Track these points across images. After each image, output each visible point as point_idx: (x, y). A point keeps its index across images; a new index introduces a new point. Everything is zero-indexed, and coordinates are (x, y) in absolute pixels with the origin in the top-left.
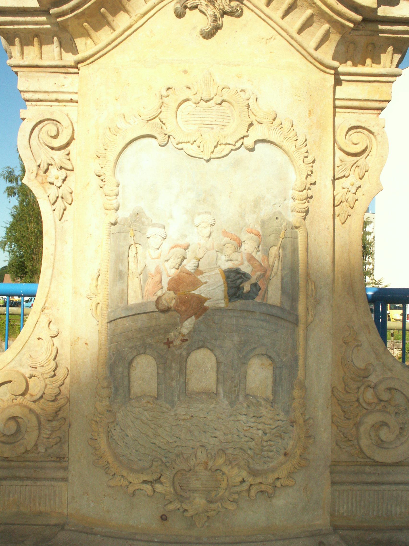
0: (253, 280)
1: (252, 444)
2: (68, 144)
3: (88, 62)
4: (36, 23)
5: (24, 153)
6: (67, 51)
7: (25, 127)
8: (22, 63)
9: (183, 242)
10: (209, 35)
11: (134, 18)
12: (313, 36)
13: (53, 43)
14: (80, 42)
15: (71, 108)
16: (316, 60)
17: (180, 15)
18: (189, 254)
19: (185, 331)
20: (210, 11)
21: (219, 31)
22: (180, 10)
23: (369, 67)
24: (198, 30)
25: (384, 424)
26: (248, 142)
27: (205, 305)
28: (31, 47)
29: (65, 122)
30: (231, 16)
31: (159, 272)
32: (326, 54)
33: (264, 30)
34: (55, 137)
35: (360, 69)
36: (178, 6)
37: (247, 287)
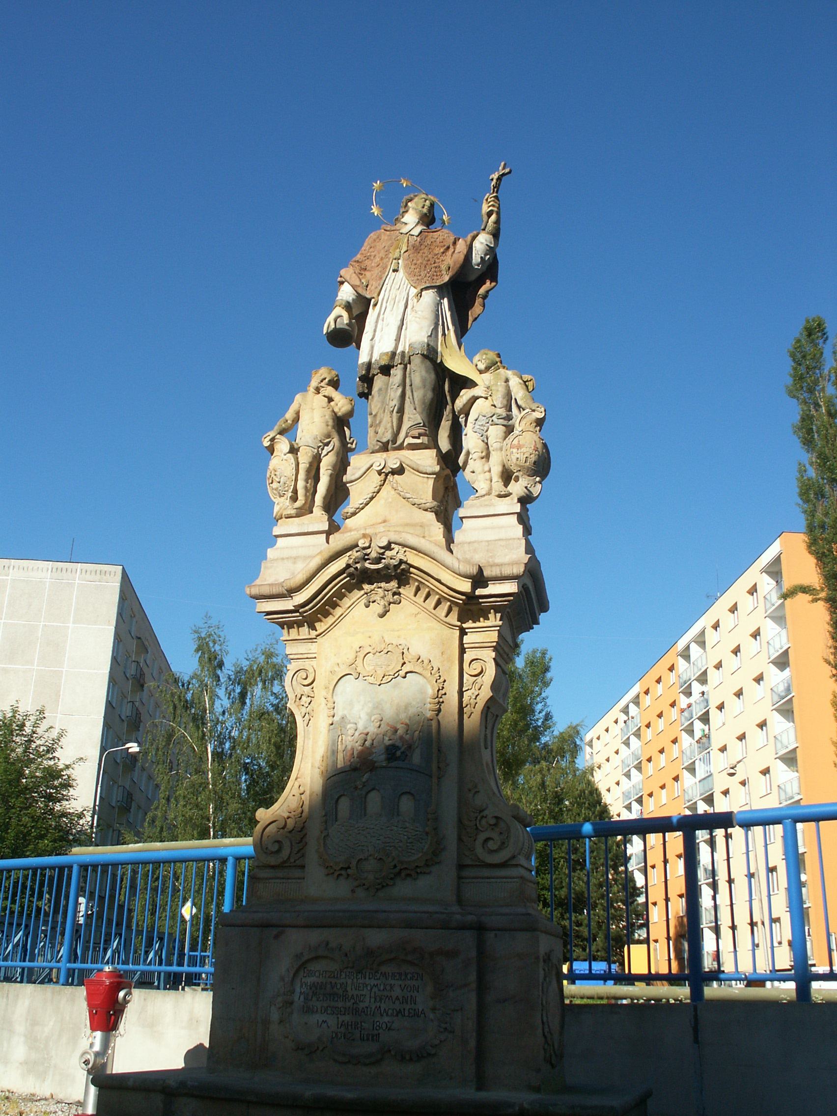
0: (402, 749)
1: (401, 844)
2: (312, 683)
4: (310, 609)
5: (288, 689)
7: (289, 674)
9: (365, 731)
10: (382, 616)
14: (317, 625)
15: (314, 663)
17: (367, 606)
18: (369, 738)
19: (364, 780)
20: (382, 602)
23: (482, 623)
25: (487, 840)
26: (402, 673)
29: (311, 670)
31: (353, 749)
32: (453, 618)
33: (413, 609)
34: (306, 679)
37: (398, 753)
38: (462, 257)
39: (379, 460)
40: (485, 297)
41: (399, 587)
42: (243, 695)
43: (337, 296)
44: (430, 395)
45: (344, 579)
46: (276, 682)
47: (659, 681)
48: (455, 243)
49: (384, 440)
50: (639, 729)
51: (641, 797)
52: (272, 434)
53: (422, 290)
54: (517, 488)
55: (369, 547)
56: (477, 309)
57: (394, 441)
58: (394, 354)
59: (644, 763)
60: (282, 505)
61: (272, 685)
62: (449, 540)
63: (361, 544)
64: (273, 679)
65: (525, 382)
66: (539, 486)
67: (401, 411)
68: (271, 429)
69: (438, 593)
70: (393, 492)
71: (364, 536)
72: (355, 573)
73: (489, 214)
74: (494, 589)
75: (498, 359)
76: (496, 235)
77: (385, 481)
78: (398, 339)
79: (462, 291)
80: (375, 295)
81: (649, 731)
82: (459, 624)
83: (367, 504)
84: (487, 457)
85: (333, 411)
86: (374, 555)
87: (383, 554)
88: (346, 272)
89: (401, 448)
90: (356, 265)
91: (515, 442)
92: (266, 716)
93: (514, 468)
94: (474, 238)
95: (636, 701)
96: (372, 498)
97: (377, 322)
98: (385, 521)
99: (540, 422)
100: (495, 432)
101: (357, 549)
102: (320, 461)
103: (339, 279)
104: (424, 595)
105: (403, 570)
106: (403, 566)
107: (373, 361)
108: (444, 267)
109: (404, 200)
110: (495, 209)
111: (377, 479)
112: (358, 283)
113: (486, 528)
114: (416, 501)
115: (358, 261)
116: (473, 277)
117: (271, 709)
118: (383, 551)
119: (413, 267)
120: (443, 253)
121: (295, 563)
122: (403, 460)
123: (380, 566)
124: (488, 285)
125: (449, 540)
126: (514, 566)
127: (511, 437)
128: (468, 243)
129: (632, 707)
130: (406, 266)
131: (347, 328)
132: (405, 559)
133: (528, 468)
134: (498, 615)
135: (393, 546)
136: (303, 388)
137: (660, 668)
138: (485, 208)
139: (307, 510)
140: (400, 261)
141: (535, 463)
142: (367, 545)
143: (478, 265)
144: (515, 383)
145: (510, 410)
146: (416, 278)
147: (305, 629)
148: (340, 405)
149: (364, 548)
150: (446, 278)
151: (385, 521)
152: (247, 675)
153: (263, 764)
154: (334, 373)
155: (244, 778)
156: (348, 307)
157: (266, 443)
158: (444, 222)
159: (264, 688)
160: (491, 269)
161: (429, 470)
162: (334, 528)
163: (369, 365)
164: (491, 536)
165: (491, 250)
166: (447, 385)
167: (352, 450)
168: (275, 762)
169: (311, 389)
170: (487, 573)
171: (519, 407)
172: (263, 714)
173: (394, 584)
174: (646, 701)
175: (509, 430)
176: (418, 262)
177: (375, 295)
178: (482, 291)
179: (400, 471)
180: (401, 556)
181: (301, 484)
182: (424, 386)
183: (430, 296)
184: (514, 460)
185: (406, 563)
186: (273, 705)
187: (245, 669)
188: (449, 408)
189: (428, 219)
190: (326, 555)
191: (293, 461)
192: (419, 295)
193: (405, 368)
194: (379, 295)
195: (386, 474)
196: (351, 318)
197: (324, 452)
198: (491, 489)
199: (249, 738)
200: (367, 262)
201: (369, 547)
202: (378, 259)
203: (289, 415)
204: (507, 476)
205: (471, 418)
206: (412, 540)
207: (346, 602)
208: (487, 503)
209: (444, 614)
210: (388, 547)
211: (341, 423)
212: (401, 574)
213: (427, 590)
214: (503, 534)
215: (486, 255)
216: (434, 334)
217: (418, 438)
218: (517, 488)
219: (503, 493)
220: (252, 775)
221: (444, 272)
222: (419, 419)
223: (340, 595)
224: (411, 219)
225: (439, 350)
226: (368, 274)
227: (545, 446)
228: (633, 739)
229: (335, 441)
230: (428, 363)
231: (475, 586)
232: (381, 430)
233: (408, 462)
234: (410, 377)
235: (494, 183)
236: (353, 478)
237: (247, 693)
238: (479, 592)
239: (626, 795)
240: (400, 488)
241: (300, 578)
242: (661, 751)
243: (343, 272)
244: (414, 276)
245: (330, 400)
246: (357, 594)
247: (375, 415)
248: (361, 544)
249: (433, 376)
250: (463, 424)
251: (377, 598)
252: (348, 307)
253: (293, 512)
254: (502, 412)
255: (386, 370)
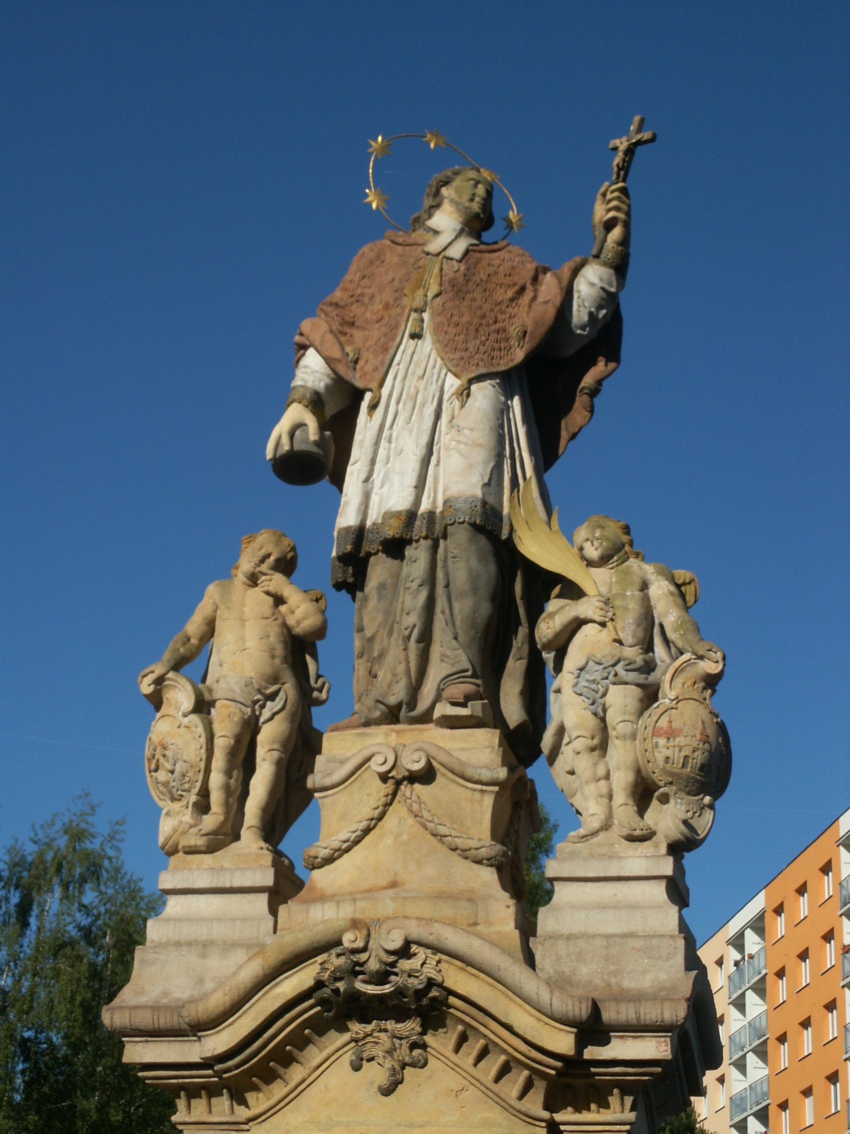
3: (260, 1120)
6: (239, 1104)
8: (187, 1119)
10: (388, 1091)
11: (308, 1071)
12: (515, 1082)
13: (222, 1095)
14: (250, 1097)
16: (519, 1111)
17: (357, 1068)
20: (388, 1063)
21: (400, 1086)
22: (357, 1063)
24: (376, 1086)
27: (692, 1098)
28: (198, 1100)
30: (415, 1067)
32: (534, 1104)
33: (453, 1080)
35: (585, 1116)
36: (354, 1058)
38: (551, 313)
39: (383, 744)
40: (594, 392)
41: (424, 1033)
42: (24, 909)
43: (293, 376)
44: (486, 608)
45: (310, 1010)
46: (88, 886)
47: (801, 890)
48: (535, 280)
49: (393, 700)
50: (763, 979)
51: (766, 1108)
52: (158, 670)
53: (471, 382)
54: (667, 818)
55: (364, 949)
56: (577, 415)
57: (412, 703)
58: (411, 516)
59: (772, 1044)
60: (174, 820)
61: (81, 893)
62: (527, 927)
63: (348, 940)
64: (83, 880)
65: (678, 586)
66: (708, 815)
67: (426, 638)
68: (157, 659)
69: (504, 1051)
70: (411, 821)
71: (355, 924)
72: (334, 998)
73: (609, 225)
74: (622, 1048)
75: (625, 539)
76: (620, 267)
77: (394, 794)
78: (420, 486)
79: (548, 381)
80: (374, 385)
81: (782, 984)
82: (546, 1115)
83: (357, 842)
84: (602, 747)
85: (285, 625)
86: (373, 965)
87: (393, 964)
88: (313, 327)
89: (425, 718)
90: (333, 312)
91: (663, 723)
92: (68, 951)
93: (659, 778)
94: (575, 272)
95: (758, 925)
96: (367, 831)
97: (377, 443)
98: (394, 885)
99: (711, 682)
100: (621, 700)
101: (338, 950)
102: (256, 730)
103: (297, 338)
104: (475, 1053)
105: (434, 999)
106: (434, 993)
107: (369, 523)
108: (514, 331)
109: (433, 182)
110: (621, 216)
111: (378, 791)
112: (336, 353)
113: (602, 907)
114: (459, 842)
115: (337, 305)
116: (570, 350)
117: (74, 933)
118: (392, 959)
119: (452, 330)
120: (512, 300)
121: (203, 956)
122: (433, 752)
123: (387, 989)
124: (600, 368)
125: (527, 927)
126: (667, 1005)
127: (655, 710)
128: (565, 283)
129: (751, 937)
130: (437, 329)
131: (315, 449)
132: (439, 979)
133: (689, 779)
134: (629, 1100)
135: (414, 948)
136: (223, 571)
137: (805, 866)
138: (600, 212)
139: (227, 834)
140: (426, 316)
141: (702, 767)
142: (360, 944)
143: (583, 328)
144: (660, 589)
145: (648, 647)
146: (458, 355)
147: (223, 1103)
148: (299, 613)
149: (354, 951)
150: (519, 355)
151: (394, 885)
152: (34, 872)
153: (56, 1039)
154: (286, 542)
155: (20, 1067)
156: (316, 402)
157: (146, 687)
158: (510, 225)
159: (66, 897)
160: (607, 336)
161: (486, 775)
162: (285, 887)
163: (359, 533)
164: (611, 924)
165: (610, 300)
166: (517, 591)
167: (319, 703)
168: (80, 1039)
169: (240, 578)
170: (609, 1015)
171: (667, 641)
172: (63, 946)
173: (412, 1026)
174: (779, 926)
175: (650, 695)
176: (465, 319)
177: (374, 385)
178: (588, 380)
179: (427, 776)
180: (429, 971)
181: (216, 780)
182: (475, 590)
183: (484, 395)
184: (661, 762)
185: (440, 986)
186: (80, 928)
187: (29, 859)
188: (523, 631)
189: (479, 224)
190: (273, 958)
191: (201, 729)
192: (464, 393)
193: (435, 547)
194: (381, 385)
195: (398, 781)
196: (322, 427)
197: (266, 714)
198: (610, 816)
199: (32, 993)
200: (356, 309)
201: (364, 949)
202: (378, 306)
203: (194, 626)
204: (644, 793)
205: (572, 661)
206: (454, 940)
207: (314, 1055)
208: (605, 850)
209: (515, 1092)
210: (404, 952)
211: (298, 648)
212: (430, 1008)
213: (482, 1042)
214: (635, 923)
215: (600, 307)
216: (494, 481)
217: (464, 705)
218: (667, 818)
219: (638, 833)
220: (36, 1063)
221: (514, 342)
222: (463, 661)
223: (300, 1041)
224: (445, 221)
225: (506, 511)
226: (358, 335)
227: (722, 729)
228: (751, 998)
229: (289, 689)
230: (483, 541)
231: (581, 1043)
232: (383, 674)
233: (443, 758)
234: (445, 567)
235: (618, 159)
236: (328, 781)
237: (30, 904)
238: (591, 1053)
239: (737, 1103)
240: (426, 814)
241: (218, 1001)
242: (805, 1024)
243: (306, 325)
244: (455, 353)
245: (279, 600)
246: (336, 1040)
247: (371, 640)
248: (348, 940)
249: (492, 568)
250: (550, 666)
251: (378, 1052)
252: (316, 402)
253: (201, 842)
254: (632, 653)
255: (395, 548)
